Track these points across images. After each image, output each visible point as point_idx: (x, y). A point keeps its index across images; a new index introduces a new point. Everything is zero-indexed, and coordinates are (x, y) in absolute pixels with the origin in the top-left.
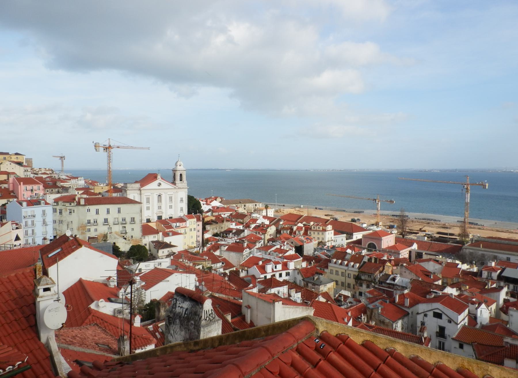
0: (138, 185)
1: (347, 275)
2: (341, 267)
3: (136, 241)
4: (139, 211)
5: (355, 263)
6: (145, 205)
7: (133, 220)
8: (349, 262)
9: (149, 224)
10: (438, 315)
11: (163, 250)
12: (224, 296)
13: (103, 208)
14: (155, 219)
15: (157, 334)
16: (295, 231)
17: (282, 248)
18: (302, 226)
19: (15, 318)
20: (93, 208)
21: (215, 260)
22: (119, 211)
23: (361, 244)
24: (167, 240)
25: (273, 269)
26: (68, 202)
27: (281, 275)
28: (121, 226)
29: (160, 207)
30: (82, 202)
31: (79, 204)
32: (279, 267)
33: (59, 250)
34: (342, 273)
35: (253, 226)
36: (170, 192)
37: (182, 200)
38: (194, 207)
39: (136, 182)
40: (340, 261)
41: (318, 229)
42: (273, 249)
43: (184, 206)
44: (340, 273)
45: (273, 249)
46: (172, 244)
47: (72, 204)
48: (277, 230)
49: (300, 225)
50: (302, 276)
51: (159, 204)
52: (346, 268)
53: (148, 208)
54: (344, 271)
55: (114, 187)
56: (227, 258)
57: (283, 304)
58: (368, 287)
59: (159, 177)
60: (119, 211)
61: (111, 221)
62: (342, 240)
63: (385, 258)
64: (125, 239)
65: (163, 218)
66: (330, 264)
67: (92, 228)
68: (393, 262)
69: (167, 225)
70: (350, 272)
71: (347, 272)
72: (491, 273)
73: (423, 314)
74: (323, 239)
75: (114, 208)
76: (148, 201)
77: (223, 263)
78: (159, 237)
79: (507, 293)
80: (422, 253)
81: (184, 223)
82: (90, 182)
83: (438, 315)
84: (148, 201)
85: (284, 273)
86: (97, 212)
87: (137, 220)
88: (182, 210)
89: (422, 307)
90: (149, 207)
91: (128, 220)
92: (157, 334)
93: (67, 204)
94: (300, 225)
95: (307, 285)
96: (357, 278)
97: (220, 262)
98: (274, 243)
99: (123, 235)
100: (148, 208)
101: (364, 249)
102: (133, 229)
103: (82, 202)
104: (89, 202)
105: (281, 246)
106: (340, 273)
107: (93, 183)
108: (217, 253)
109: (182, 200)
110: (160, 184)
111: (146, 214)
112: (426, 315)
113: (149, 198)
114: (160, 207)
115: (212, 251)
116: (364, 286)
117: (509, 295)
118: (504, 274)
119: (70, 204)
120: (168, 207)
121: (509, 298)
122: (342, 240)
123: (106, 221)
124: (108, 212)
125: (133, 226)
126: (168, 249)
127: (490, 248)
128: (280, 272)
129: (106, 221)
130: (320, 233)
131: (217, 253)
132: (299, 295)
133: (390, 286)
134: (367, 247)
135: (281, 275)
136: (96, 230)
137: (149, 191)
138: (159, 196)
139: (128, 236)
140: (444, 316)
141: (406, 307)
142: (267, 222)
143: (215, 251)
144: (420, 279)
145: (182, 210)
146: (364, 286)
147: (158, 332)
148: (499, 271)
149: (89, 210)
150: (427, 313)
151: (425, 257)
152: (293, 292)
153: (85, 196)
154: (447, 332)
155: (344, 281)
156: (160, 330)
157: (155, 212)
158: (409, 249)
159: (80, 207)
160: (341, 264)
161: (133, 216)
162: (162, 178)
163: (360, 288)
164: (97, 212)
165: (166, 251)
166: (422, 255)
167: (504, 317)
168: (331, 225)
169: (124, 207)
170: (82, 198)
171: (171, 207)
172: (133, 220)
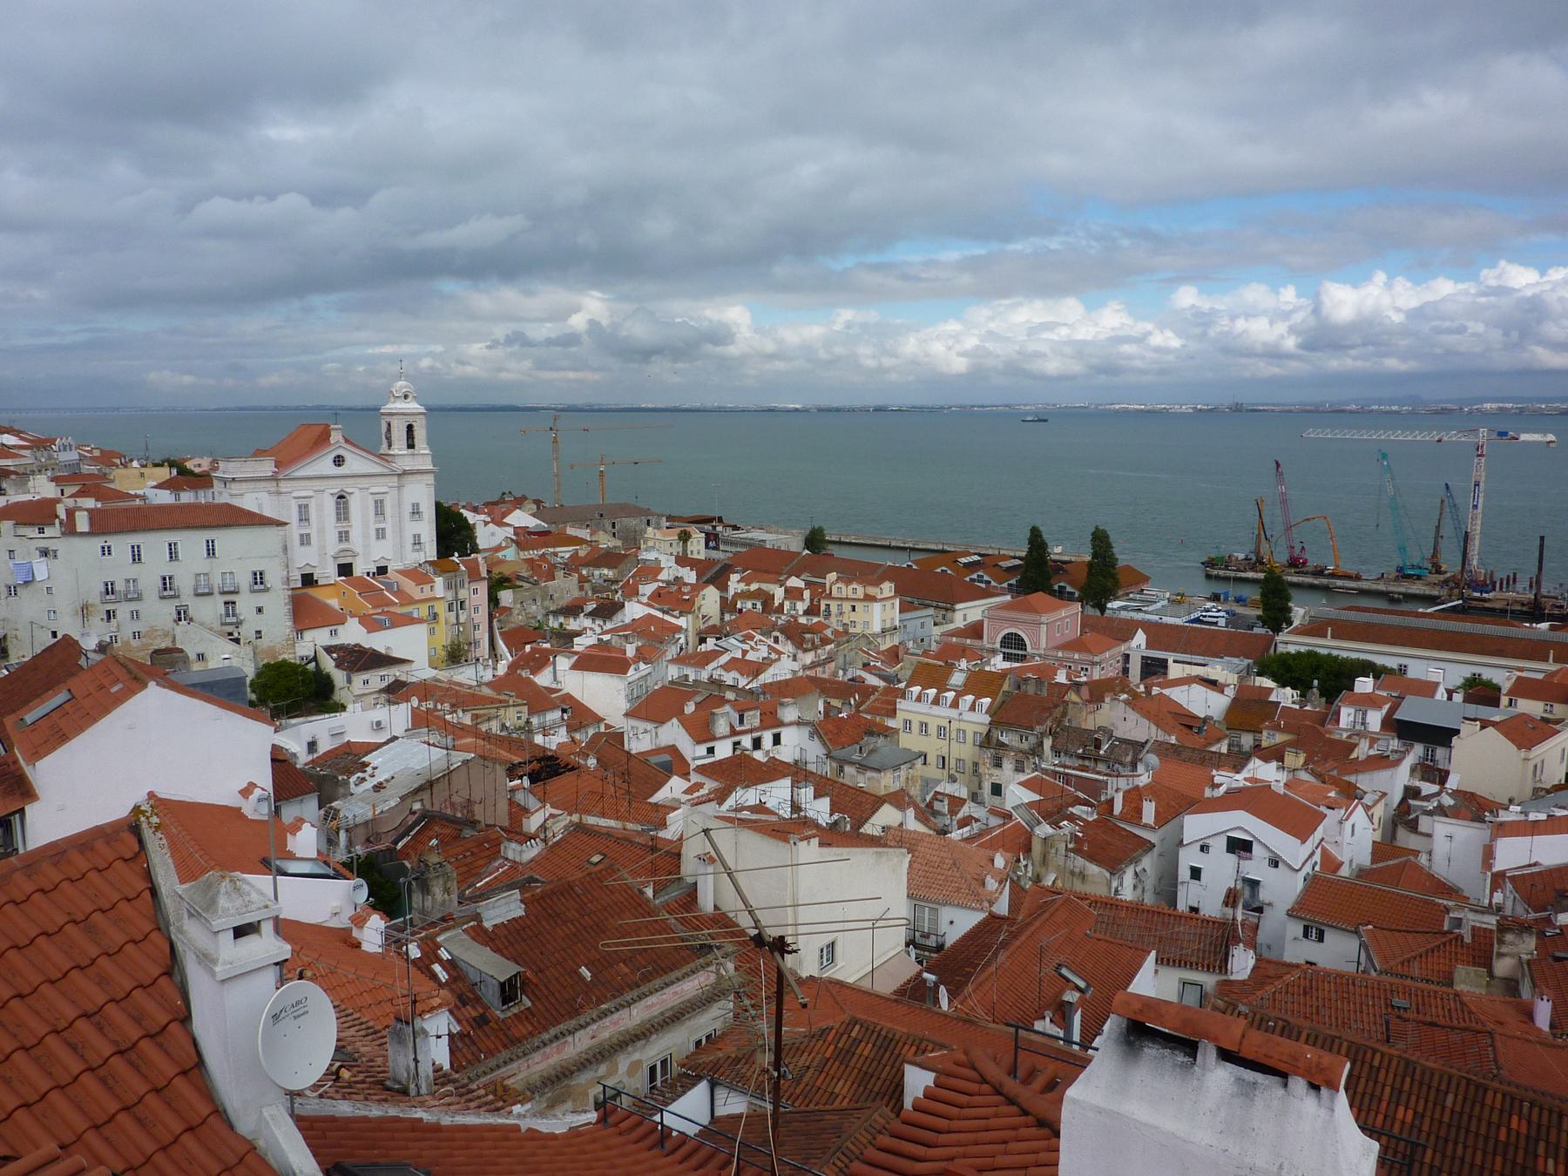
0: (267, 467)
1: (954, 735)
2: (936, 710)
3: (271, 651)
4: (278, 548)
5: (979, 696)
6: (295, 530)
7: (258, 578)
8: (959, 694)
9: (311, 591)
10: (1239, 847)
11: (365, 676)
12: (612, 823)
13: (154, 544)
14: (327, 573)
15: (437, 968)
16: (782, 605)
17: (748, 657)
18: (802, 584)
19: (115, 1042)
20: (121, 544)
21: (540, 700)
22: (211, 552)
23: (980, 637)
24: (379, 642)
25: (732, 727)
26: (32, 524)
27: (757, 744)
28: (221, 600)
29: (344, 536)
30: (82, 524)
31: (70, 530)
32: (753, 719)
33: (60, 698)
34: (940, 728)
35: (647, 589)
36: (379, 487)
37: (416, 512)
38: (453, 534)
39: (259, 453)
40: (932, 692)
41: (851, 595)
42: (724, 659)
43: (427, 529)
44: (933, 730)
45: (724, 659)
46: (395, 655)
47: (49, 532)
48: (723, 600)
49: (794, 582)
50: (824, 744)
51: (343, 526)
52: (953, 713)
53: (305, 540)
54: (945, 723)
55: (183, 471)
56: (577, 695)
57: (821, 844)
58: (1019, 769)
59: (336, 437)
60: (211, 552)
61: (184, 583)
62: (922, 625)
63: (1061, 677)
64: (237, 641)
65: (358, 571)
66: (902, 705)
67: (123, 611)
68: (1085, 691)
69: (378, 594)
70: (963, 726)
71: (955, 725)
72: (1365, 714)
73: (1197, 846)
74: (867, 623)
75: (191, 543)
76: (304, 518)
77: (564, 711)
78: (352, 633)
79: (1413, 770)
80: (1166, 661)
81: (427, 587)
82: (97, 453)
83: (1239, 847)
84: (304, 518)
85: (767, 738)
86: (136, 557)
87: (274, 578)
88: (417, 542)
89: (1195, 826)
90: (308, 535)
91: (244, 580)
92: (437, 968)
93: (32, 532)
94: (794, 582)
95: (842, 770)
96: (987, 742)
97: (553, 708)
98: (722, 643)
99: (230, 629)
100: (305, 540)
101: (994, 652)
102: (260, 610)
103: (82, 524)
104: (102, 525)
105: (745, 652)
106: (933, 730)
107: (107, 458)
108: (543, 679)
109: (416, 512)
110: (339, 461)
111: (304, 559)
112: (1204, 848)
113: (306, 506)
114: (344, 536)
115: (525, 673)
116: (1008, 765)
117: (1418, 774)
118: (1400, 715)
119: (41, 531)
120: (373, 533)
121: (1417, 783)
122: (922, 625)
123: (166, 582)
124: (173, 555)
125: (261, 600)
126: (383, 672)
127: (1362, 640)
128: (755, 735)
129: (166, 582)
130: (859, 606)
131: (543, 679)
132: (824, 804)
133: (1087, 763)
134: (998, 645)
135: (757, 744)
136: (135, 615)
137: (308, 483)
138: (341, 497)
139: (247, 632)
140: (1256, 848)
141: (1146, 826)
142: (690, 576)
143: (535, 671)
144: (1173, 740)
145: (417, 542)
146: (1008, 765)
147: (440, 961)
148: (1387, 707)
149: (106, 551)
150: (1210, 841)
151: (1175, 671)
152: (806, 793)
153: (90, 503)
154: (1264, 895)
155: (945, 752)
156: (445, 955)
157: (332, 552)
158: (1123, 648)
159: (76, 542)
160: (936, 702)
161: (258, 568)
162: (347, 441)
163: (996, 771)
164: (136, 557)
165: (377, 679)
166: (1166, 667)
167: (1405, 839)
168: (891, 580)
169: (230, 541)
170: (81, 509)
171: (381, 534)
172: (258, 578)
